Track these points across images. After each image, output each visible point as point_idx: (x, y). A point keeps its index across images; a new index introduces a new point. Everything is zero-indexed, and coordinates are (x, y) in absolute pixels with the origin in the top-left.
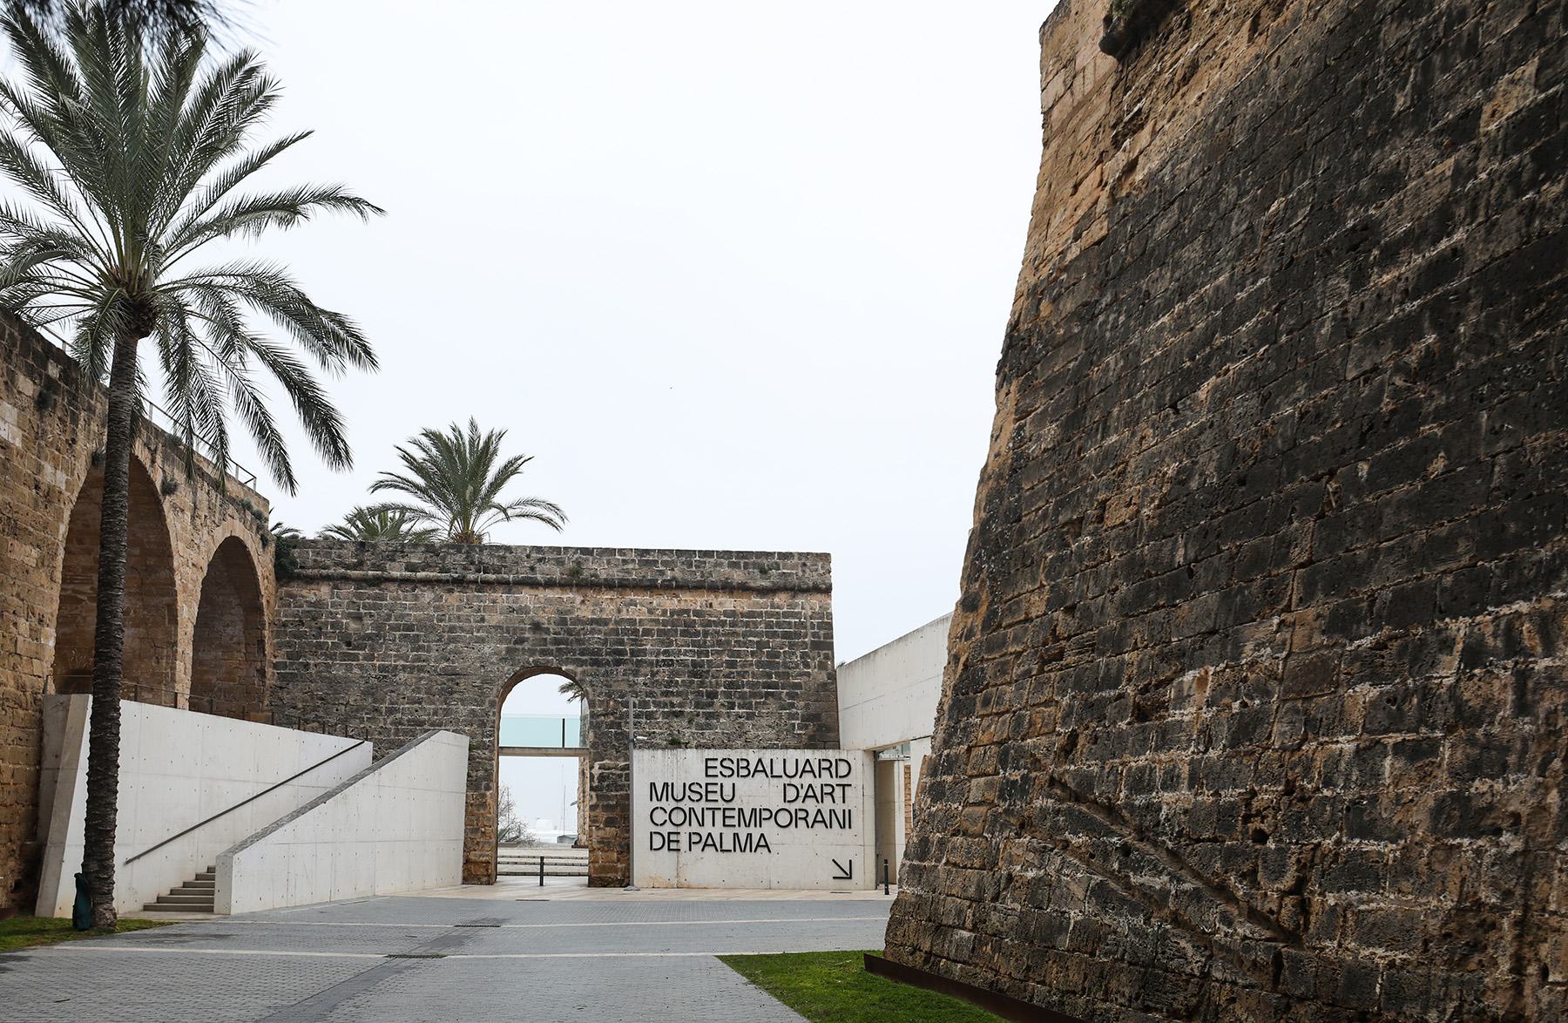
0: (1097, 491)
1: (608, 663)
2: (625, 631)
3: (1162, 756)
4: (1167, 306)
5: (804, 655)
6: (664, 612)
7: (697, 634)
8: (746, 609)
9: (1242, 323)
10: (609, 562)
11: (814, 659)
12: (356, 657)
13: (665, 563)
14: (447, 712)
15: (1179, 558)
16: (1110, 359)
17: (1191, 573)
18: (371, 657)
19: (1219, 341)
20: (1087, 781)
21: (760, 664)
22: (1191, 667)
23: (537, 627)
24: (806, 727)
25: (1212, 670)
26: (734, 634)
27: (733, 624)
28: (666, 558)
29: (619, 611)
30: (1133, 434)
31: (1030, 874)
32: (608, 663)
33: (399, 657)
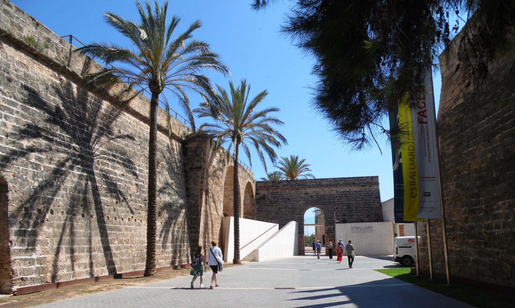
0: (467, 161)
1: (328, 204)
2: (332, 197)
3: (494, 221)
4: (484, 118)
5: (373, 200)
6: (340, 192)
7: (348, 196)
8: (359, 190)
9: (507, 121)
10: (327, 181)
11: (376, 201)
12: (273, 206)
13: (340, 181)
14: (293, 217)
15: (494, 175)
16: (468, 130)
17: (498, 179)
18: (276, 206)
19: (500, 125)
20: (472, 228)
21: (363, 203)
22: (500, 201)
23: (312, 197)
24: (375, 217)
25: (507, 201)
26: (357, 196)
27: (356, 194)
28: (340, 180)
29: (330, 192)
30: (477, 147)
31: (458, 249)
32: (328, 204)
33: (282, 205)
